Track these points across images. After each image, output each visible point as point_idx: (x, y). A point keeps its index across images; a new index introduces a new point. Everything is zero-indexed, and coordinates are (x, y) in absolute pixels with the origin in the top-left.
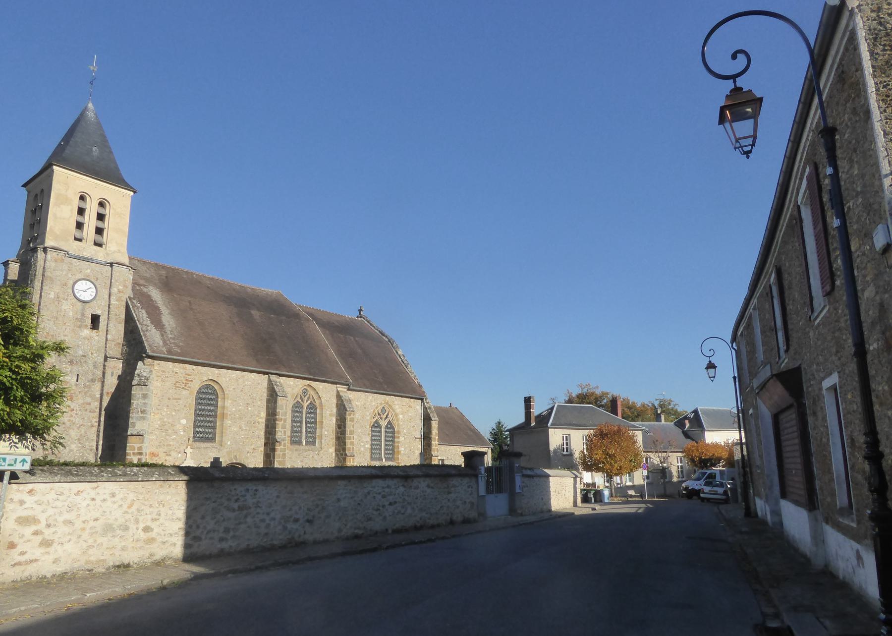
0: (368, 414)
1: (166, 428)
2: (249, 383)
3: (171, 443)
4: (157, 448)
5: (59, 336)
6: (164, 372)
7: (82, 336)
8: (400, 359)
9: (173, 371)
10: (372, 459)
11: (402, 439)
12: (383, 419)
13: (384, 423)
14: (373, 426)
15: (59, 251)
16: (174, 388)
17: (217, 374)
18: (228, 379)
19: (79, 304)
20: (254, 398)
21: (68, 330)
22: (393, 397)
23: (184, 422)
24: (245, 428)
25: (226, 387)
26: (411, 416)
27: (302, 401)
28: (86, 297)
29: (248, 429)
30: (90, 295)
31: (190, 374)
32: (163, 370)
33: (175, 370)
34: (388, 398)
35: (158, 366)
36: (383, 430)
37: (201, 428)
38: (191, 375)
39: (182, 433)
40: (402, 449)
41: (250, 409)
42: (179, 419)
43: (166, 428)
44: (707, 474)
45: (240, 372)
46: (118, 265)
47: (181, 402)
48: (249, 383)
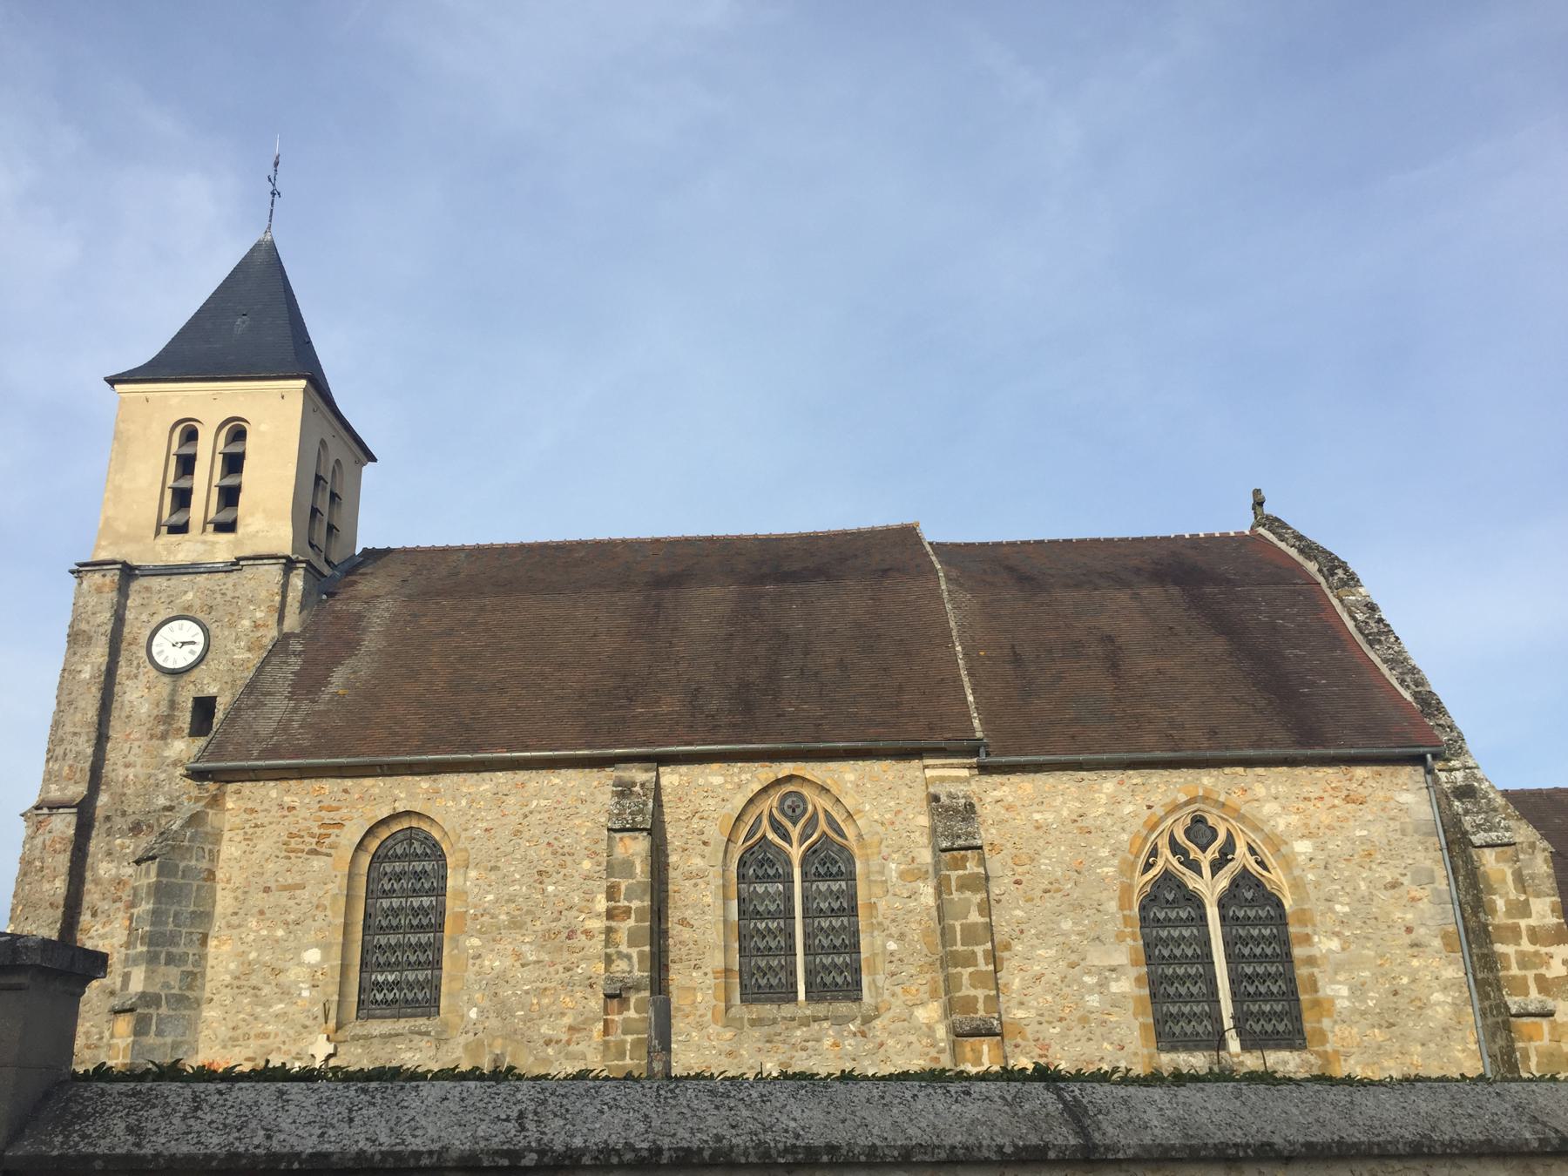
0: (1104, 853)
1: (255, 980)
2: (543, 803)
3: (269, 1028)
4: (224, 1047)
5: (113, 770)
6: (253, 811)
7: (167, 757)
8: (1350, 625)
9: (281, 806)
10: (1166, 1034)
11: (1326, 945)
12: (1206, 871)
13: (1210, 887)
14: (1151, 900)
15: (105, 567)
16: (284, 854)
17: (427, 791)
18: (464, 802)
19: (167, 679)
20: (566, 850)
21: (135, 750)
22: (1240, 770)
23: (313, 956)
24: (534, 958)
25: (458, 830)
26: (1363, 840)
27: (786, 837)
28: (178, 658)
29: (546, 958)
30: (162, 651)
31: (334, 804)
32: (250, 805)
33: (287, 799)
34: (1206, 780)
35: (235, 797)
36: (1213, 913)
37: (392, 972)
38: (338, 809)
39: (305, 993)
40: (1337, 991)
41: (551, 888)
42: (298, 950)
43: (255, 980)
44: (786, 845)
45: (510, 774)
46: (251, 562)
47: (304, 895)
48: (543, 803)
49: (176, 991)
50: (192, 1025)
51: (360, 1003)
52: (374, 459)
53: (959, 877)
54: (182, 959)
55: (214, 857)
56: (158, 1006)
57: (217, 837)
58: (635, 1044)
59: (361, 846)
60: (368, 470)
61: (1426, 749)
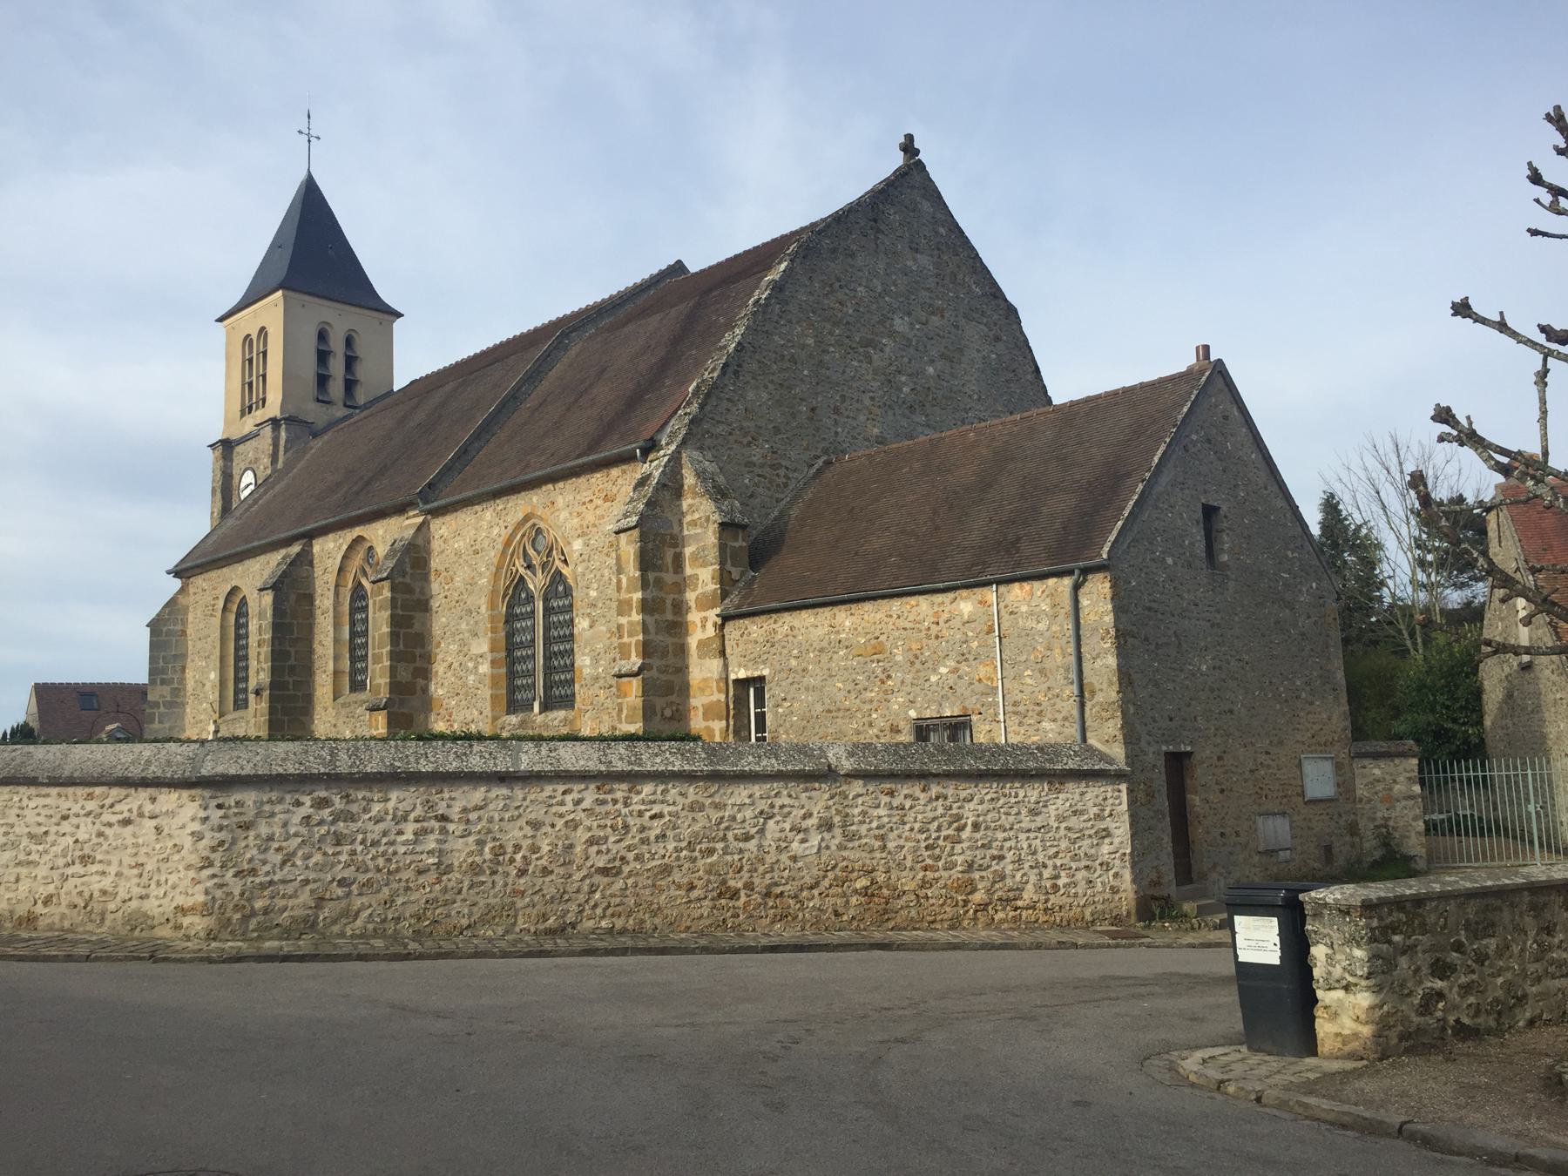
49: (168, 699)
50: (182, 717)
51: (235, 702)
52: (399, 315)
53: (380, 600)
54: (171, 681)
55: (184, 622)
56: (159, 707)
57: (186, 609)
58: (152, 721)
59: (225, 609)
60: (398, 325)
61: (633, 446)
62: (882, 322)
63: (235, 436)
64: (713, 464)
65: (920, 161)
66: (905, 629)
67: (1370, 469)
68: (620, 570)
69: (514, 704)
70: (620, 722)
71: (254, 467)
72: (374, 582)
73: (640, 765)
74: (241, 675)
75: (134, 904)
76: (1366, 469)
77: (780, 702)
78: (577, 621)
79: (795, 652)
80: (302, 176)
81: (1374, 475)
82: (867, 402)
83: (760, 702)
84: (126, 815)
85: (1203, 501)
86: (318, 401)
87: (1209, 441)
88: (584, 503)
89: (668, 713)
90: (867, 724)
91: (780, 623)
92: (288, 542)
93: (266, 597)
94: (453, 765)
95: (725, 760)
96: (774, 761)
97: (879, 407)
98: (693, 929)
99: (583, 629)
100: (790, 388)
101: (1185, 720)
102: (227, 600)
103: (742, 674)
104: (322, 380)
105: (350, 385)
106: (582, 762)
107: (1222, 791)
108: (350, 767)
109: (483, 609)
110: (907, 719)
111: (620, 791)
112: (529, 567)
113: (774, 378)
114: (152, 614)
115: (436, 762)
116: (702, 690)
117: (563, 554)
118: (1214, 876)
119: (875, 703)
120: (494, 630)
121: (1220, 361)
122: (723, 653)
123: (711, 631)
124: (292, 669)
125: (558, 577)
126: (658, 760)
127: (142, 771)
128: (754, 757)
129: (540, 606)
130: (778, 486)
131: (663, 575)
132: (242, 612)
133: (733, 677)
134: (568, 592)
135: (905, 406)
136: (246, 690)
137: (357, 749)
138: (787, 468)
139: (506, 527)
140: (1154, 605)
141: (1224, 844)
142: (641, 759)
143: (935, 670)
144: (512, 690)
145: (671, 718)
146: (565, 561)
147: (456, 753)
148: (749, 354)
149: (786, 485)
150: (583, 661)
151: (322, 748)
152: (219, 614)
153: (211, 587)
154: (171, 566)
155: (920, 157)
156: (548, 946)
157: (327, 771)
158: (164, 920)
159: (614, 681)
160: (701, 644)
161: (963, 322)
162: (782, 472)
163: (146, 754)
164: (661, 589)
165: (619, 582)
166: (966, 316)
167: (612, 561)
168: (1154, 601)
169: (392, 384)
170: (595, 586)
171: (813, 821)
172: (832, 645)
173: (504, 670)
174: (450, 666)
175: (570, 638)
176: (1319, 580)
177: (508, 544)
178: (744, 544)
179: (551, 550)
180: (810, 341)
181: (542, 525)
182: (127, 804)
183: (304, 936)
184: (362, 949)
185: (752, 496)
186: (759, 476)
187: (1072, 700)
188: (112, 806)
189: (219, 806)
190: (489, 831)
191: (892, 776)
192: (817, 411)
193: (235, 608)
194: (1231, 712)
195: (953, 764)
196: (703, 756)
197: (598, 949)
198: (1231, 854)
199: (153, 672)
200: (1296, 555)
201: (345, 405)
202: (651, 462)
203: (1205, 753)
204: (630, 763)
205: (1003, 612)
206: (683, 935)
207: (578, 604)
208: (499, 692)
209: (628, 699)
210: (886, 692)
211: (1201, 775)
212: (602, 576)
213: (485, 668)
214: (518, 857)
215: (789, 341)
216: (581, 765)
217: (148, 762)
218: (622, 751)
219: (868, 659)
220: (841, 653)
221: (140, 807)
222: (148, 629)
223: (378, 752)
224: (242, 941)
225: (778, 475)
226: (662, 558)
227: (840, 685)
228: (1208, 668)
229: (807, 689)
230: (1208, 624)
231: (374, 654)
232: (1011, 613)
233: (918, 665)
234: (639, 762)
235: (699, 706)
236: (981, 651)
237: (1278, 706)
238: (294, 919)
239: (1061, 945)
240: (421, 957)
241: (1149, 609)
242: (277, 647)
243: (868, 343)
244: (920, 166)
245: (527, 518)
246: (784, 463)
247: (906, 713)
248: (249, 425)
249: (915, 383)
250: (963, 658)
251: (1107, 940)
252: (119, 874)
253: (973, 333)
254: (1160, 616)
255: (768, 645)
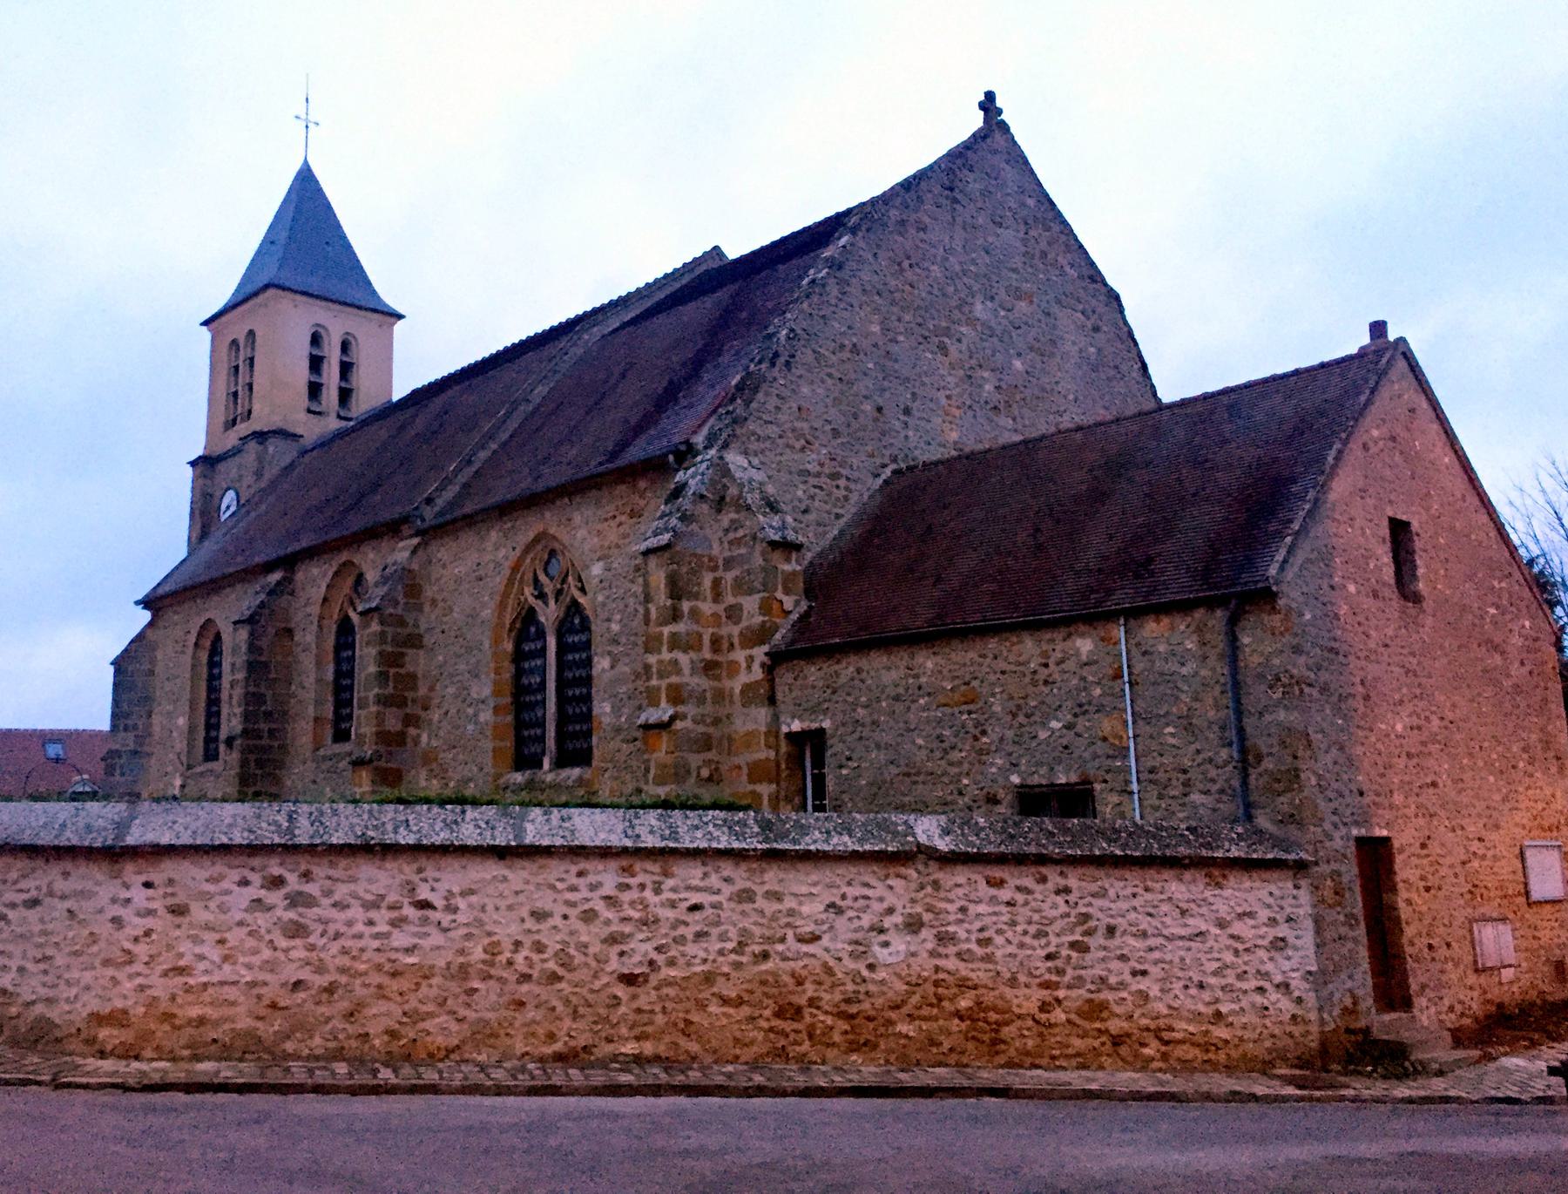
52: (400, 317)
62: (959, 308)
63: (218, 450)
64: (761, 472)
65: (1003, 122)
66: (1003, 673)
67: (1548, 490)
68: (647, 598)
69: (525, 759)
70: (647, 783)
71: (237, 485)
72: (362, 614)
73: (676, 840)
74: (213, 721)
75: (39, 1009)
76: (1543, 491)
77: (844, 762)
78: (596, 659)
79: (863, 699)
80: (297, 166)
81: (1554, 498)
82: (944, 401)
83: (819, 762)
84: (34, 893)
85: (1391, 514)
86: (309, 411)
87: (1393, 439)
88: (606, 520)
89: (705, 773)
90: (955, 792)
91: (844, 664)
92: (268, 567)
93: (241, 631)
94: (441, 837)
95: (784, 836)
96: (846, 838)
97: (958, 407)
98: (743, 1059)
99: (603, 670)
100: (851, 383)
101: (1378, 795)
102: (200, 635)
103: (796, 726)
104: (315, 390)
105: (345, 395)
106: (602, 836)
107: (1428, 889)
108: (312, 837)
109: (487, 644)
110: (1008, 787)
111: (646, 873)
112: (541, 596)
113: (832, 371)
114: (117, 650)
115: (419, 831)
116: (748, 746)
117: (580, 580)
118: (1423, 1002)
119: (966, 766)
120: (497, 672)
121: (1402, 341)
122: (772, 700)
123: (758, 673)
124: (268, 715)
125: (575, 607)
126: (699, 834)
127: (56, 837)
128: (821, 833)
129: (552, 643)
130: (838, 499)
131: (699, 604)
132: (216, 650)
133: (785, 729)
134: (585, 626)
135: (988, 407)
136: (216, 739)
137: (322, 813)
138: (848, 479)
139: (514, 549)
140: (1336, 645)
141: (1433, 959)
142: (677, 833)
143: (1044, 725)
144: (520, 742)
145: (710, 779)
146: (583, 590)
147: (444, 821)
148: (802, 342)
149: (846, 498)
150: (603, 709)
151: (279, 811)
152: (190, 650)
153: (186, 623)
154: (140, 597)
155: (1003, 117)
156: (557, 1079)
157: (283, 841)
158: (73, 1031)
159: (639, 734)
160: (747, 688)
161: (1055, 309)
162: (842, 482)
163: (62, 817)
164: (697, 622)
165: (647, 612)
166: (1059, 302)
167: (637, 589)
168: (1335, 640)
169: (390, 394)
170: (618, 617)
171: (897, 919)
172: (910, 691)
173: (510, 718)
174: (446, 713)
175: (587, 681)
176: (1532, 618)
177: (515, 568)
178: (798, 568)
179: (567, 575)
180: (876, 328)
181: (557, 546)
182: (35, 879)
183: (247, 1056)
184: (321, 1077)
185: (805, 511)
186: (815, 487)
187: (1230, 767)
188: (15, 882)
189: (148, 885)
190: (480, 923)
191: (1001, 860)
192: (884, 411)
193: (208, 644)
194: (1434, 784)
195: (1079, 847)
196: (756, 829)
197: (620, 1086)
198: (1442, 972)
199: (119, 714)
200: (1503, 585)
201: (339, 417)
202: (687, 469)
203: (1404, 838)
204: (663, 838)
205: (1134, 651)
206: (730, 1068)
207: (597, 640)
208: (502, 744)
209: (655, 755)
210: (981, 752)
211: (1406, 870)
212: (626, 606)
213: (486, 716)
214: (519, 958)
215: (850, 328)
216: (600, 840)
217: (64, 826)
218: (654, 822)
219: (956, 710)
220: (922, 701)
221: (49, 885)
222: (112, 669)
223: (347, 818)
224: (168, 1060)
225: (838, 487)
226: (699, 584)
227: (920, 742)
228: (1405, 727)
229: (878, 746)
230: (1402, 671)
231: (359, 699)
232: (1145, 653)
233: (1021, 719)
234: (674, 835)
235: (743, 764)
236: (1106, 701)
237: (1492, 779)
238: (236, 1034)
239: (1235, 1096)
240: (392, 1090)
241: (1331, 650)
242: (252, 689)
243: (947, 332)
244: (1004, 128)
245: (537, 540)
246: (844, 472)
247: (1007, 778)
248: (232, 439)
249: (1000, 380)
250: (1081, 710)
251: (1290, 1090)
252: (21, 970)
253: (1068, 321)
254: (1341, 658)
255: (829, 691)
